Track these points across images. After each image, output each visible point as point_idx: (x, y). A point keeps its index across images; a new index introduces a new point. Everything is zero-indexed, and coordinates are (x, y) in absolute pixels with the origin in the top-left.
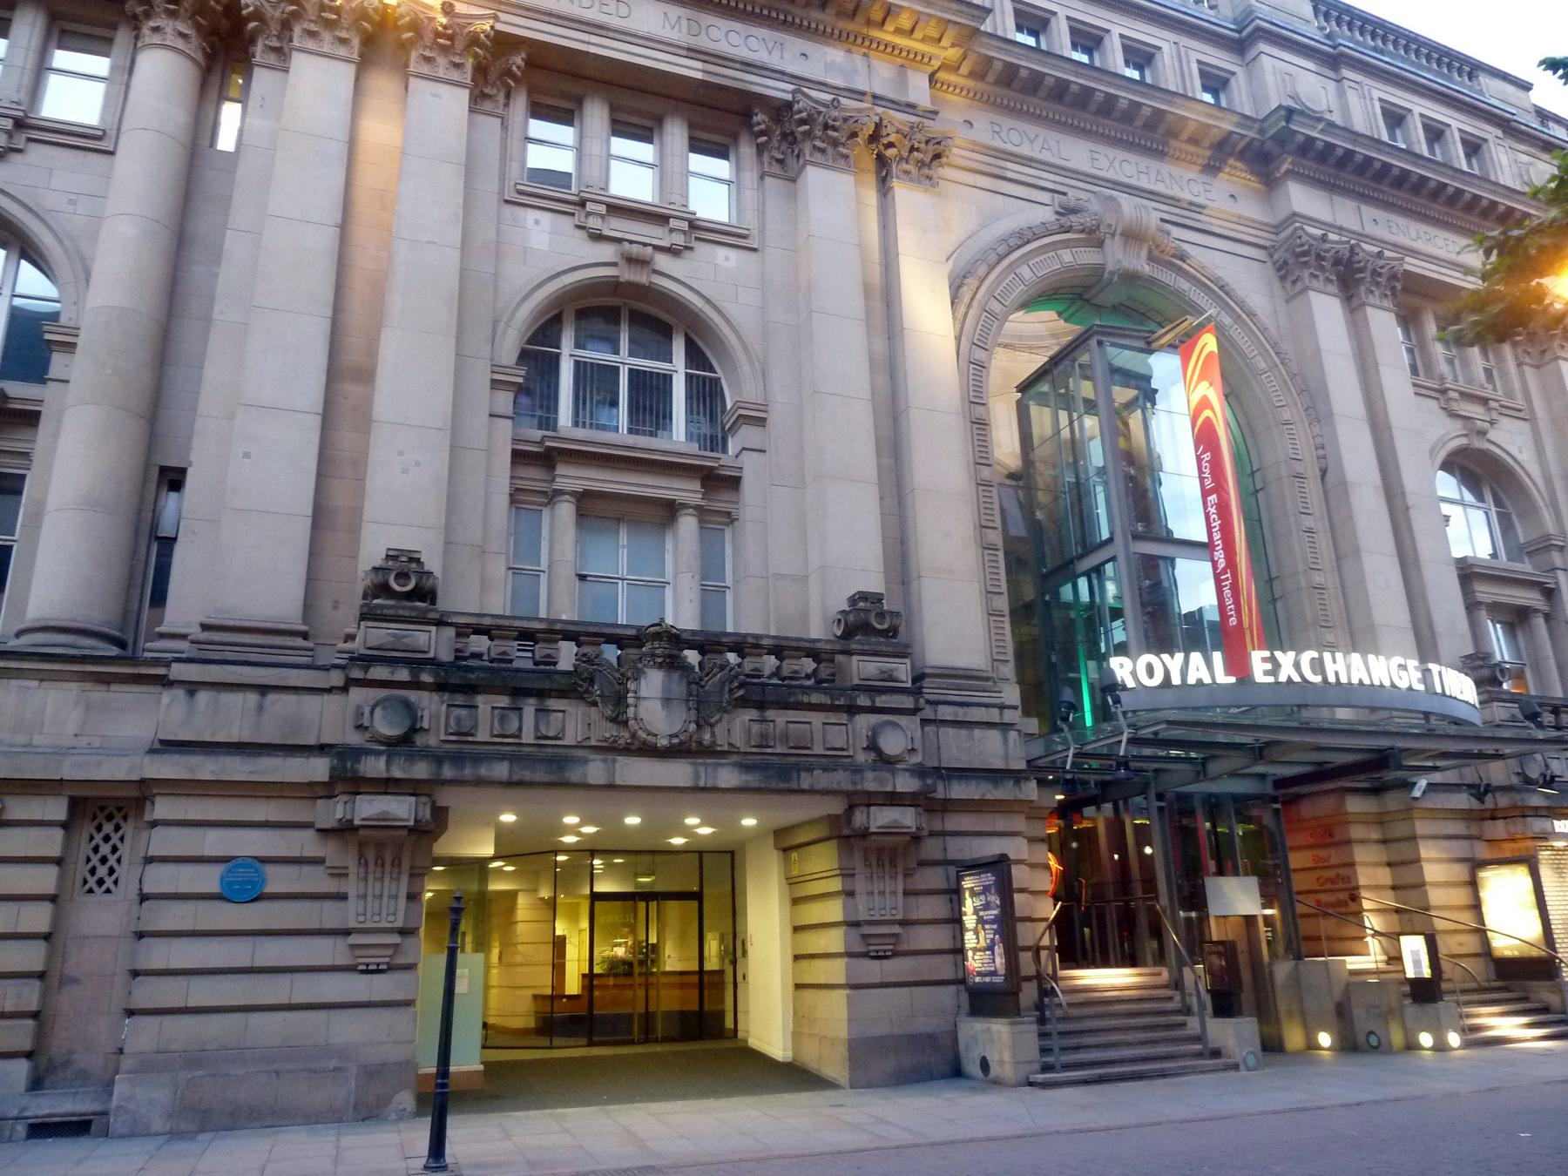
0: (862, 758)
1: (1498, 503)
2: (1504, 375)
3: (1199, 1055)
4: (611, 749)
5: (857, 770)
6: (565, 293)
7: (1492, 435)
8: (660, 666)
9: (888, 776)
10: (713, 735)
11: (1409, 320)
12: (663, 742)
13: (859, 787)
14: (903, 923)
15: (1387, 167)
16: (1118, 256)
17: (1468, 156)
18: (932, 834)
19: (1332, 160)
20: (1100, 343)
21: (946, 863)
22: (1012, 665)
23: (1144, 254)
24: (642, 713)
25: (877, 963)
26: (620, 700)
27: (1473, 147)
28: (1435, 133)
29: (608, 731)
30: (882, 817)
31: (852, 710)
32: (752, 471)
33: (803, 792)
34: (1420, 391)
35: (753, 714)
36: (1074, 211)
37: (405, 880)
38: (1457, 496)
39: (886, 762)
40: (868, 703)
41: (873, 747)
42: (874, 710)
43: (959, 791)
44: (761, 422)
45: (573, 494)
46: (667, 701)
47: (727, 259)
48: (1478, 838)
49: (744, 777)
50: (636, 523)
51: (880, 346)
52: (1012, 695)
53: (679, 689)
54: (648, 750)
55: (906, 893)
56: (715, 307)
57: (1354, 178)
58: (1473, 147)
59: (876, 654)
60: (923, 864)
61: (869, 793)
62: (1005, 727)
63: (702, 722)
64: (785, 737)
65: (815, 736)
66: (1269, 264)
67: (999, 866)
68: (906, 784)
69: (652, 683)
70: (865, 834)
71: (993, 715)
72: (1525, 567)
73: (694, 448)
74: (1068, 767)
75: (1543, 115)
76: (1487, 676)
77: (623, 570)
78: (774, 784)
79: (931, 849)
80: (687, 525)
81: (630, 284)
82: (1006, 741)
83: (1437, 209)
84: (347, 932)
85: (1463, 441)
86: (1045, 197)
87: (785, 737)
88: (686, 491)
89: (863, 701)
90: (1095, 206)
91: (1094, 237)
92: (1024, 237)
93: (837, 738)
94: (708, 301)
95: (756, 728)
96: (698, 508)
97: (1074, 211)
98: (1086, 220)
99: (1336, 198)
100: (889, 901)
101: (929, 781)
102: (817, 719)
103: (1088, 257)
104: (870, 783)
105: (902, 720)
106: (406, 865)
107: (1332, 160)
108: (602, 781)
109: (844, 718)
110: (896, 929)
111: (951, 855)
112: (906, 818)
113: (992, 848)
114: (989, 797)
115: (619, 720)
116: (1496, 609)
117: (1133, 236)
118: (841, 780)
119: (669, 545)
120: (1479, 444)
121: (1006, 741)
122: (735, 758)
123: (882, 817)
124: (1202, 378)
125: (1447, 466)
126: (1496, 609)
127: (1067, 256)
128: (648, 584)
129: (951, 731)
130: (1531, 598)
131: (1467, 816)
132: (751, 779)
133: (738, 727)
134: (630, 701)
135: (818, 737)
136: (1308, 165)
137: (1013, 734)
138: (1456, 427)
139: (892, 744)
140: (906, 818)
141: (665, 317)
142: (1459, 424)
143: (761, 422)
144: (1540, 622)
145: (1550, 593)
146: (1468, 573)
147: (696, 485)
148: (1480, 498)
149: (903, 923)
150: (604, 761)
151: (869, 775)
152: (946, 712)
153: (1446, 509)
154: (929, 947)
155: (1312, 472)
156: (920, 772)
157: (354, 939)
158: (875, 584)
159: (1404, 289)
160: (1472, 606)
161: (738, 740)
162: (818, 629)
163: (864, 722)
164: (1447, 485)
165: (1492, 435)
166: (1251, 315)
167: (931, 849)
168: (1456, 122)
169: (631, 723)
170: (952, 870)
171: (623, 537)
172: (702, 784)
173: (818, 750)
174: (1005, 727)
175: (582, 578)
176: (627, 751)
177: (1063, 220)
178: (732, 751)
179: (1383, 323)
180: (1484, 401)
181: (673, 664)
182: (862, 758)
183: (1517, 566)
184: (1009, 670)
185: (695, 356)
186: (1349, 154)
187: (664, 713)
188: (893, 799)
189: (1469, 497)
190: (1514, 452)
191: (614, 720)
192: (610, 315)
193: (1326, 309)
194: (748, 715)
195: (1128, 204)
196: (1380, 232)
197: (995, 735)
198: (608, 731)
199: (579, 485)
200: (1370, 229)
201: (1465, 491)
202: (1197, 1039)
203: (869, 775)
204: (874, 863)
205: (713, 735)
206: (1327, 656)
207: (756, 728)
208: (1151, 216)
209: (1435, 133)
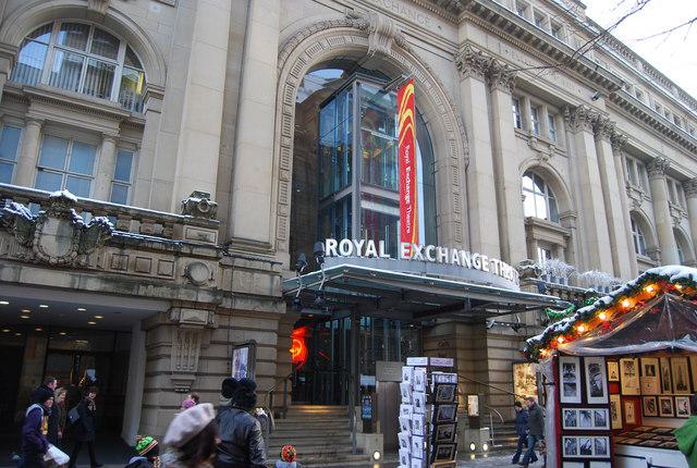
0: (180, 281)
1: (550, 194)
2: (559, 136)
3: (351, 452)
4: (21, 262)
5: (175, 287)
6: (53, 11)
7: (550, 161)
8: (58, 217)
9: (195, 293)
10: (88, 259)
11: (519, 102)
12: (53, 261)
13: (175, 297)
14: (196, 374)
15: (514, 26)
16: (375, 44)
17: (554, 32)
18: (221, 327)
19: (488, 18)
20: (358, 84)
21: (228, 343)
22: (288, 242)
23: (390, 44)
24: (42, 243)
25: (179, 395)
26: (30, 234)
27: (556, 29)
28: (540, 19)
29: (20, 251)
30: (188, 315)
31: (178, 254)
32: (150, 120)
33: (140, 297)
34: (518, 135)
35: (117, 250)
36: (356, 18)
37: (198, 350)
38: (532, 189)
39: (195, 285)
40: (188, 251)
41: (187, 275)
42: (191, 255)
43: (240, 305)
44: (160, 97)
45: (39, 121)
46: (59, 237)
47: (155, 8)
48: (517, 350)
49: (103, 285)
50: (78, 144)
51: (235, 67)
52: (284, 258)
53: (68, 231)
54: (44, 264)
55: (200, 358)
56: (143, 32)
57: (489, 23)
58: (556, 29)
59: (198, 225)
60: (213, 343)
61: (182, 301)
62: (273, 274)
63: (81, 251)
64: (135, 266)
65: (153, 267)
66: (454, 63)
67: (251, 345)
68: (204, 298)
69: (53, 226)
70: (177, 323)
71: (268, 267)
72: (558, 225)
73: (119, 106)
74: (528, 341)
75: (590, 21)
76: (526, 276)
77: (67, 167)
78: (121, 291)
79: (220, 335)
80: (108, 147)
81: (94, 12)
82: (272, 281)
83: (520, 42)
84: (170, 373)
85: (536, 162)
86: (342, 8)
87: (135, 266)
88: (111, 128)
89: (185, 250)
90: (366, 17)
91: (364, 31)
92: (326, 26)
93: (166, 268)
94: (139, 28)
95: (116, 258)
96: (115, 138)
97: (356, 18)
98: (361, 22)
99: (490, 37)
100: (190, 362)
101: (218, 298)
102: (155, 257)
103: (360, 41)
104: (183, 295)
105: (208, 263)
106: (199, 345)
107: (488, 18)
108: (11, 280)
109: (173, 258)
110: (193, 377)
111: (232, 340)
112: (202, 316)
113: (249, 336)
114: (257, 309)
115: (28, 245)
116: (542, 243)
117: (385, 35)
118: (164, 292)
119: (97, 158)
120: (544, 164)
121: (272, 281)
122: (100, 274)
123: (188, 315)
124: (407, 108)
125: (528, 173)
126: (542, 243)
127: (348, 39)
128: (79, 177)
129: (241, 273)
130: (558, 239)
131: (512, 338)
132: (109, 287)
133: (106, 256)
134: (36, 235)
135: (154, 267)
136: (476, 18)
137: (277, 278)
138: (533, 155)
139: (199, 275)
140: (202, 316)
141: (116, 35)
142: (535, 154)
143: (160, 97)
144: (561, 251)
145: (568, 239)
146: (530, 224)
147: (116, 126)
148: (543, 192)
149: (196, 374)
150: (14, 268)
151: (183, 291)
152: (239, 262)
153: (525, 193)
154: (211, 388)
155: (462, 166)
156: (214, 291)
157: (173, 377)
158: (209, 187)
159: (517, 87)
160: (530, 240)
161: (105, 265)
162: (173, 213)
163: (184, 262)
164: (528, 182)
165: (550, 161)
166: (441, 85)
167: (220, 335)
168: (549, 14)
169: (35, 248)
170: (230, 347)
171: (70, 148)
172: (76, 287)
173: (153, 274)
174: (273, 274)
175: (40, 169)
176: (31, 263)
177: (348, 21)
178: (99, 269)
179: (504, 99)
180: (549, 145)
181: (67, 217)
182: (180, 281)
183: (554, 224)
184: (285, 245)
185: (130, 55)
186: (497, 16)
187: (57, 244)
188: (196, 305)
189: (537, 189)
190: (559, 171)
191: (24, 245)
192: (85, 29)
193: (476, 87)
194: (111, 251)
195: (382, 18)
196: (508, 57)
197: (267, 277)
198: (20, 251)
199: (43, 117)
200: (504, 55)
201: (536, 187)
202: (351, 444)
203: (183, 291)
204: (191, 341)
205: (88, 259)
206: (440, 249)
207: (116, 258)
208: (396, 27)
209: (540, 19)
